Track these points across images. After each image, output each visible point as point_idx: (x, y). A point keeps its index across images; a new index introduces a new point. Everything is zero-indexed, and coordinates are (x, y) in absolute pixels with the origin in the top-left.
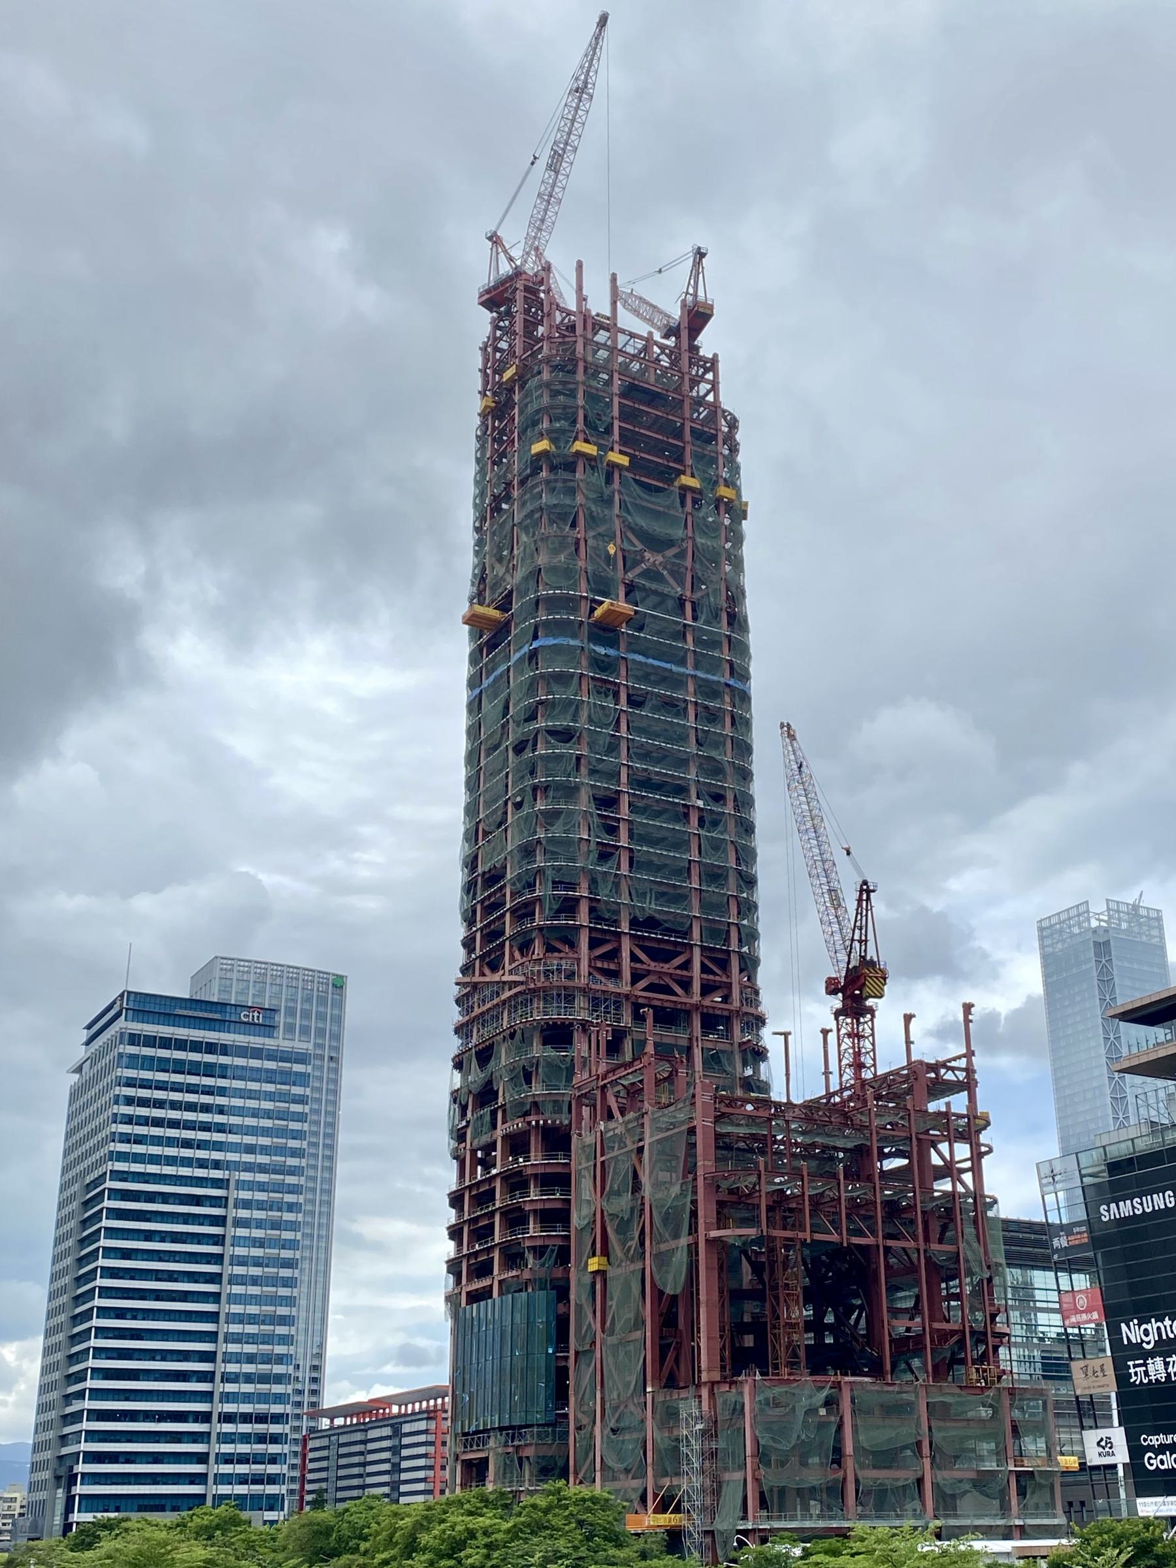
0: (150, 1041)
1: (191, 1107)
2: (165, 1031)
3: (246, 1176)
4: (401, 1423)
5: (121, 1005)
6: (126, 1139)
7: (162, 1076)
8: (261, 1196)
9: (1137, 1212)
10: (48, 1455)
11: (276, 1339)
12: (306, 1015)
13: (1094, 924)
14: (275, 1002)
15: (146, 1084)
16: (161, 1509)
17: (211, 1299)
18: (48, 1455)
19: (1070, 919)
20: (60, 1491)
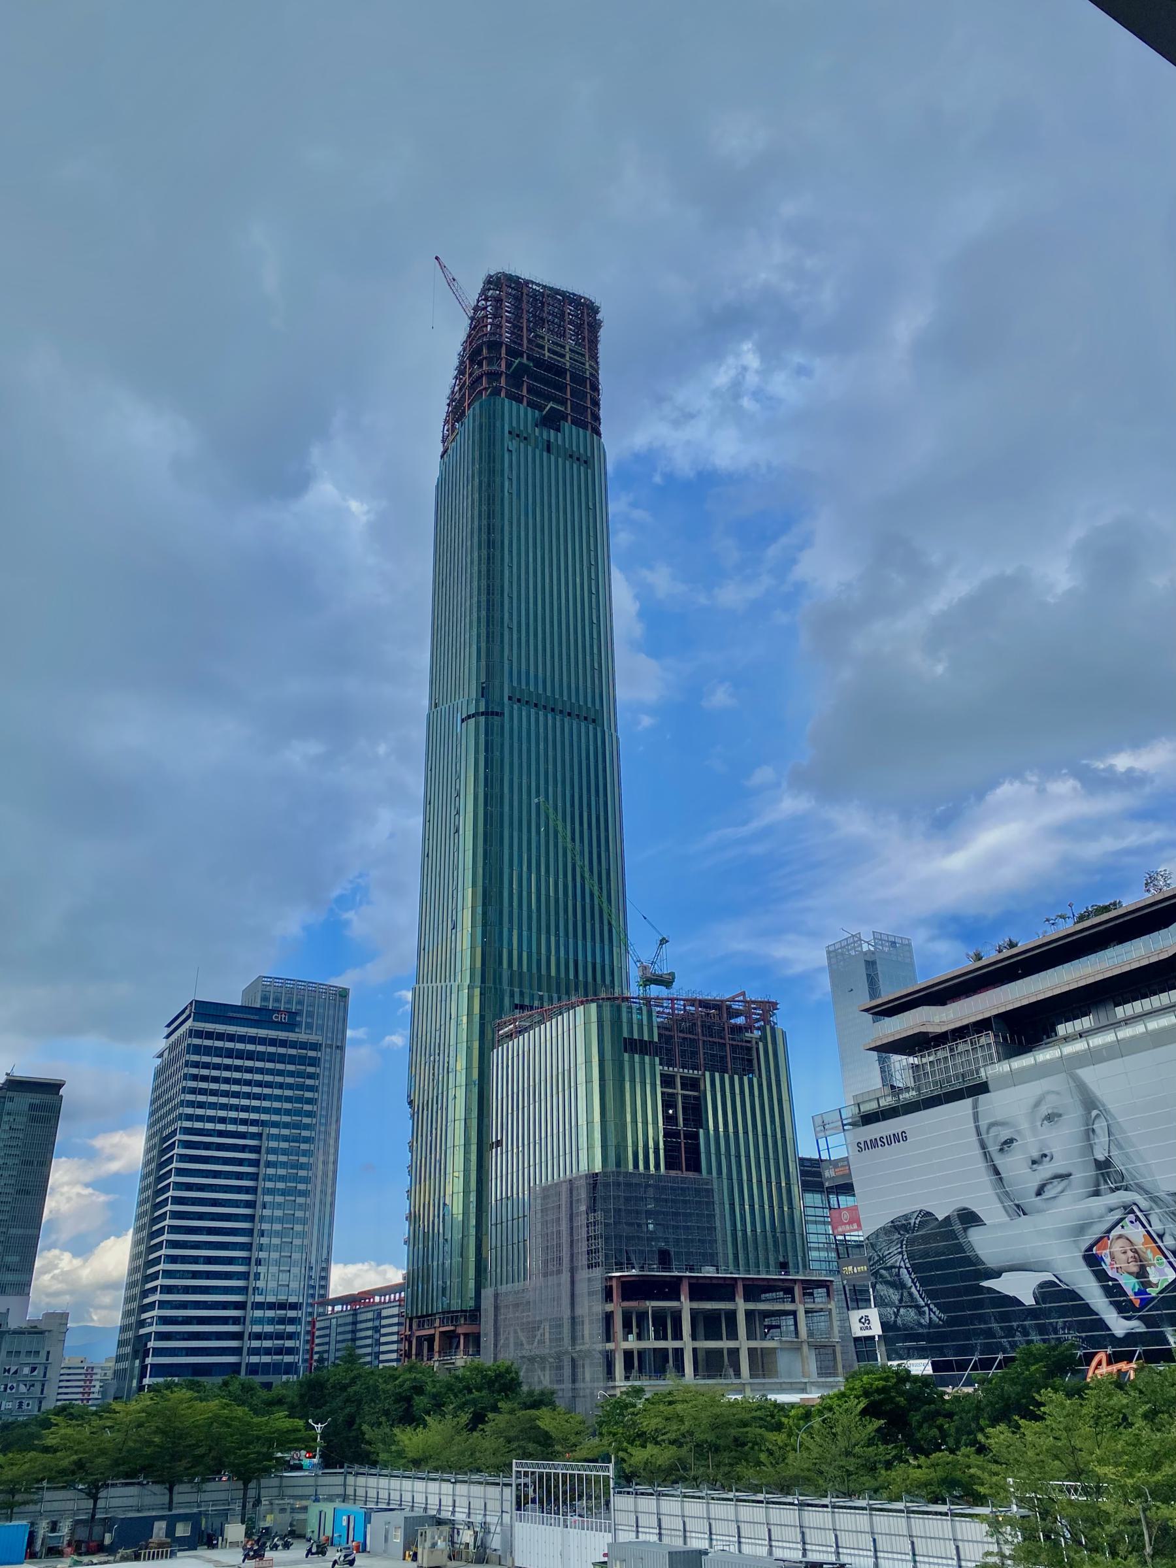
0: (209, 1035)
1: (224, 1107)
3: (274, 1131)
4: (381, 1309)
6: (191, 1104)
13: (865, 947)
14: (299, 1007)
15: (206, 1066)
19: (848, 945)
20: (137, 1362)
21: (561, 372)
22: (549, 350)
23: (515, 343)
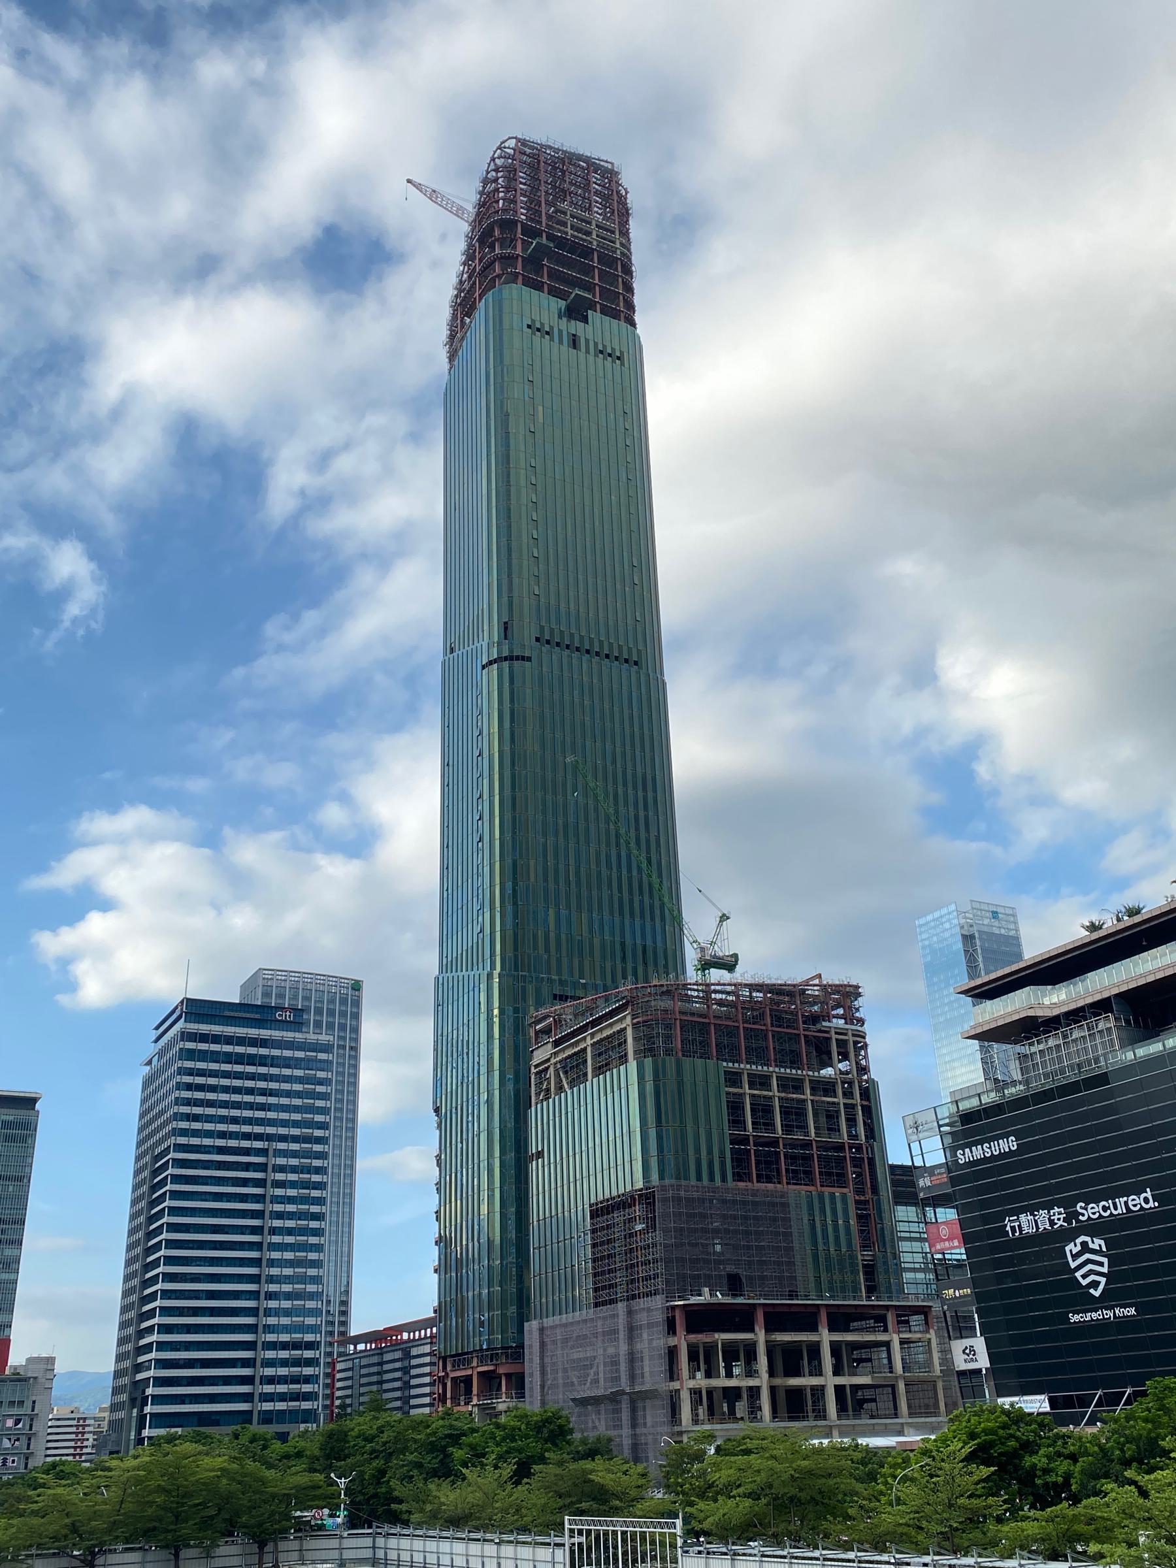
0: (204, 1038)
2: (216, 1029)
3: (282, 1146)
4: (410, 1347)
5: (182, 1009)
7: (214, 1066)
8: (294, 1162)
9: (987, 1155)
10: (126, 1380)
11: (308, 1280)
12: (343, 1014)
16: (217, 1423)
17: (255, 1247)
18: (126, 1380)
21: (587, 252)
22: (572, 227)
23: (532, 220)
